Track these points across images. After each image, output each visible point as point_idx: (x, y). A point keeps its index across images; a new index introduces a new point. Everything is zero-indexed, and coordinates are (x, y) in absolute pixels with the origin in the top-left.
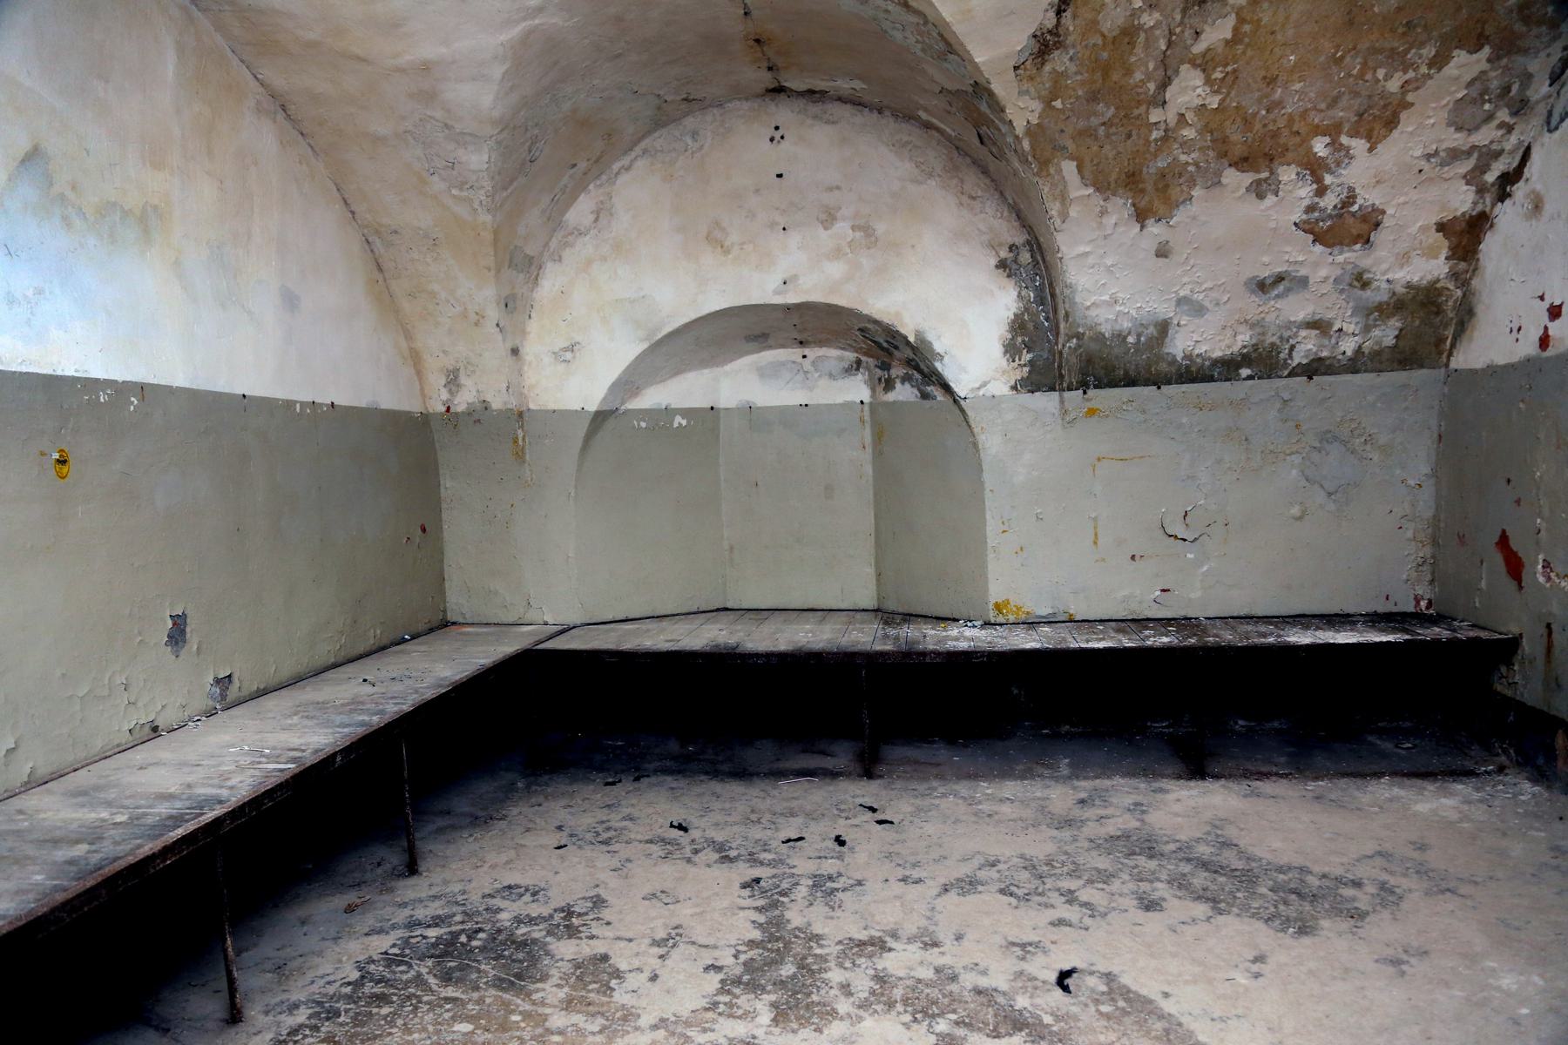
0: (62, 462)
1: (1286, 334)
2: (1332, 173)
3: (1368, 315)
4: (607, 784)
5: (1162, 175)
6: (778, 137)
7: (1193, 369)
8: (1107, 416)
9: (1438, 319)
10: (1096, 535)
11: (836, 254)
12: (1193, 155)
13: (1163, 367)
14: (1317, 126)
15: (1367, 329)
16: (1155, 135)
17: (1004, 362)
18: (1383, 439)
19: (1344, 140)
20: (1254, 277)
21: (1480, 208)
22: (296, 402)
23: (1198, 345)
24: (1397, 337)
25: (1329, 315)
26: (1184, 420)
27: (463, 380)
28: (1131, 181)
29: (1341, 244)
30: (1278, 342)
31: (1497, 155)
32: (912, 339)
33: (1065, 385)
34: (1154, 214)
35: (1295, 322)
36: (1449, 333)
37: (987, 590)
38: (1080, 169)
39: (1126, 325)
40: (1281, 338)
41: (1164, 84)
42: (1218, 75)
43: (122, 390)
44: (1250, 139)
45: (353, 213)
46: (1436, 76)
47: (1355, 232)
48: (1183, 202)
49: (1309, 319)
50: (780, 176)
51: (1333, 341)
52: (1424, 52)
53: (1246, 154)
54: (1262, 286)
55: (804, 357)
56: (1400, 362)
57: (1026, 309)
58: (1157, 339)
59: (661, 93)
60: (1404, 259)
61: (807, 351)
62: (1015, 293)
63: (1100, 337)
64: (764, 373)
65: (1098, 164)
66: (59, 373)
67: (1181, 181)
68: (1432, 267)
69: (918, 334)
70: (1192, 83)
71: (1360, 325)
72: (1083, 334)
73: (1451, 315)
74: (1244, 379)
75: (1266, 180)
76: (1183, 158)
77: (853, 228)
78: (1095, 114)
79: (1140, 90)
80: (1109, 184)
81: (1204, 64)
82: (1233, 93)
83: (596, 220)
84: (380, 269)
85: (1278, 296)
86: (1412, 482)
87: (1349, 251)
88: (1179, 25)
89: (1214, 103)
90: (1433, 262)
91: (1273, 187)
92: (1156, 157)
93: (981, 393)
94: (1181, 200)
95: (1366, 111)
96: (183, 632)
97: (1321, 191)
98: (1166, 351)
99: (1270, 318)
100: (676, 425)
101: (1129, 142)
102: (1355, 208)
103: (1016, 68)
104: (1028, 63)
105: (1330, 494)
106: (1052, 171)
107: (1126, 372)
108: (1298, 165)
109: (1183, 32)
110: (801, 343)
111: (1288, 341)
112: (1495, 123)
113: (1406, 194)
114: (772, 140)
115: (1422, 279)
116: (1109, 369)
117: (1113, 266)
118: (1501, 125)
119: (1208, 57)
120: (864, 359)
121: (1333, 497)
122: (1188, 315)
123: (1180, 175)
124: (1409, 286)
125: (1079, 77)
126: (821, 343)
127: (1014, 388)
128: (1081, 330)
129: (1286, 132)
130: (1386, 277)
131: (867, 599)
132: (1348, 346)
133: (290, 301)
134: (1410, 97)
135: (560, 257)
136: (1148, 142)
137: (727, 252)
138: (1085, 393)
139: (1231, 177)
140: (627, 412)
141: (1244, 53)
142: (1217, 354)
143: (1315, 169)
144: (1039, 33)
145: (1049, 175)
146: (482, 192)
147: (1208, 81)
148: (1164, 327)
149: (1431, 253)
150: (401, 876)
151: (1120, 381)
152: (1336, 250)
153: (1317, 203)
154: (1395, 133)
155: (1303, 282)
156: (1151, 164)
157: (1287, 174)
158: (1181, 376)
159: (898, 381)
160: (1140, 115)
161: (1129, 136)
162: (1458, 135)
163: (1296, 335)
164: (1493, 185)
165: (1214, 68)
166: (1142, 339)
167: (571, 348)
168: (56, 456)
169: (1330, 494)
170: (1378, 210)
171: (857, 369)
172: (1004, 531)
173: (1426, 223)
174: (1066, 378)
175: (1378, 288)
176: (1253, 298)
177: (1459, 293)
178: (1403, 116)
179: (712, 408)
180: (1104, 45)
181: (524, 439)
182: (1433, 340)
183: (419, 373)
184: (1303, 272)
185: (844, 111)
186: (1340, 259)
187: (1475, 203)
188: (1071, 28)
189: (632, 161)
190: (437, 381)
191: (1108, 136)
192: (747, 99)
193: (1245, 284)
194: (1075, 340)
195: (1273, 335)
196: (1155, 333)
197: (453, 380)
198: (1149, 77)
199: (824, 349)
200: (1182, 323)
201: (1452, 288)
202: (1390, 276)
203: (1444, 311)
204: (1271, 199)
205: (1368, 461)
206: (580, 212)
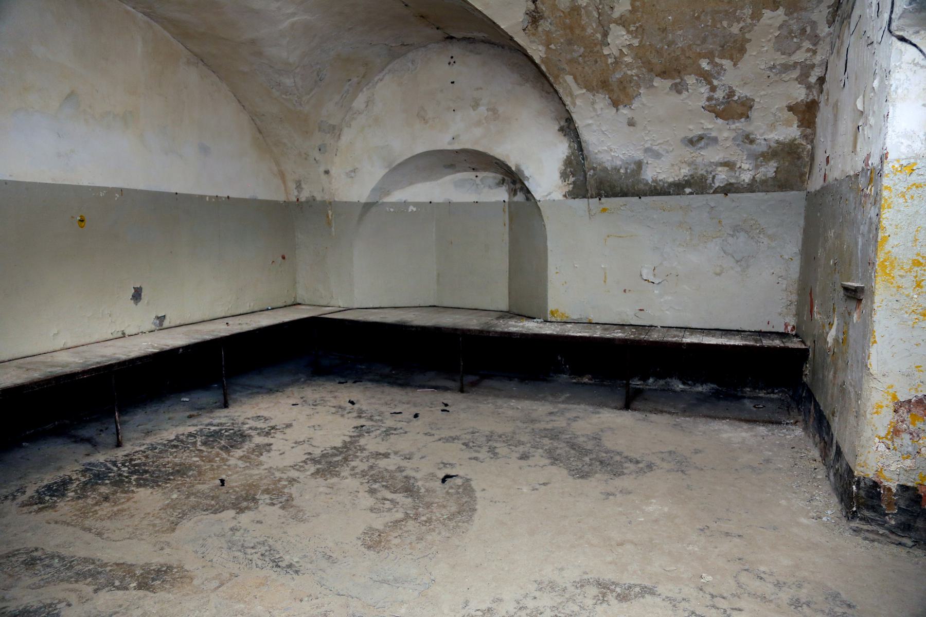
0: (82, 221)
1: (710, 169)
2: (716, 79)
3: (757, 159)
4: (340, 383)
5: (621, 82)
6: (452, 62)
7: (658, 188)
8: (613, 213)
9: (799, 162)
10: (605, 277)
11: (478, 123)
12: (634, 71)
13: (641, 186)
14: (700, 53)
15: (757, 167)
16: (610, 61)
17: (560, 182)
18: (770, 232)
19: (717, 60)
20: (685, 137)
21: (811, 97)
22: (206, 196)
23: (659, 175)
24: (775, 172)
25: (733, 159)
26: (655, 216)
27: (303, 186)
28: (605, 85)
29: (733, 118)
30: (705, 173)
31: (813, 66)
32: (514, 169)
33: (589, 195)
34: (622, 103)
35: (713, 162)
36: (807, 170)
37: (547, 303)
38: (575, 78)
39: (619, 163)
40: (707, 171)
41: (605, 35)
42: (632, 28)
43: (110, 191)
44: (663, 62)
45: (243, 106)
46: (757, 24)
47: (739, 112)
48: (636, 96)
49: (721, 160)
50: (453, 83)
51: (737, 174)
52: (745, 11)
53: (664, 70)
54: (692, 142)
55: (477, 176)
56: (779, 187)
57: (573, 153)
58: (636, 171)
59: (387, 43)
60: (772, 127)
61: (478, 174)
62: (567, 145)
63: (605, 170)
64: (458, 185)
65: (584, 77)
66: (81, 184)
67: (632, 85)
68: (790, 132)
69: (517, 167)
70: (619, 33)
71: (752, 165)
72: (596, 168)
73: (807, 160)
74: (688, 194)
75: (680, 83)
76: (629, 72)
77: (487, 110)
78: (574, 51)
79: (593, 38)
80: (593, 88)
81: (623, 22)
82: (645, 38)
83: (367, 106)
84: (260, 132)
85: (701, 148)
86: (786, 257)
87: (738, 123)
88: (600, 4)
89: (636, 43)
90: (791, 129)
91: (685, 87)
92: (614, 72)
93: (548, 198)
94: (635, 95)
95: (724, 45)
96: (140, 295)
97: (713, 89)
98: (642, 177)
99: (699, 160)
100: (410, 210)
101: (597, 64)
102: (736, 98)
103: (524, 30)
104: (529, 27)
105: (737, 261)
106: (561, 81)
107: (621, 189)
108: (696, 75)
109: (603, 7)
110: (474, 169)
111: (711, 173)
112: (804, 49)
113: (764, 90)
114: (449, 64)
115: (785, 139)
116: (612, 187)
117: (606, 131)
118: (808, 50)
119: (623, 19)
120: (506, 178)
121: (739, 263)
122: (651, 158)
123: (631, 82)
124: (778, 142)
125: (558, 33)
126: (485, 170)
127: (565, 196)
128: (595, 165)
129: (683, 58)
130: (763, 137)
131: (504, 305)
132: (746, 177)
133: (204, 150)
134: (747, 36)
135: (350, 125)
136: (607, 65)
137: (426, 123)
138: (600, 199)
139: (657, 82)
140: (383, 203)
141: (642, 16)
142: (671, 180)
143: (706, 77)
144: (528, 12)
145: (560, 83)
146: (296, 96)
147: (628, 32)
148: (639, 165)
149: (788, 123)
150: (220, 408)
151: (619, 194)
152: (730, 122)
153: (713, 96)
154: (746, 56)
155: (715, 140)
156: (613, 76)
157: (691, 80)
158: (652, 191)
159: (518, 190)
160: (598, 51)
161: (596, 62)
162: (783, 57)
163: (714, 170)
164: (815, 84)
165: (629, 25)
166: (628, 171)
167: (354, 171)
168: (79, 218)
169: (737, 261)
170: (750, 99)
171: (503, 184)
172: (557, 273)
173: (780, 106)
174: (590, 191)
175: (760, 144)
176: (688, 149)
177: (809, 147)
178: (748, 46)
179: (431, 202)
180: (565, 16)
181: (332, 216)
182: (798, 174)
183: (284, 182)
184: (714, 134)
185: (482, 47)
186: (733, 126)
187: (807, 95)
188: (544, 9)
189: (384, 76)
190: (292, 186)
191: (585, 62)
192: (438, 43)
193: (681, 141)
194: (592, 171)
195: (702, 170)
196: (635, 168)
197: (299, 186)
198: (596, 32)
199: (487, 173)
200: (649, 162)
201: (805, 144)
202: (766, 137)
203: (802, 157)
204: (685, 94)
205: (761, 244)
206: (359, 102)
